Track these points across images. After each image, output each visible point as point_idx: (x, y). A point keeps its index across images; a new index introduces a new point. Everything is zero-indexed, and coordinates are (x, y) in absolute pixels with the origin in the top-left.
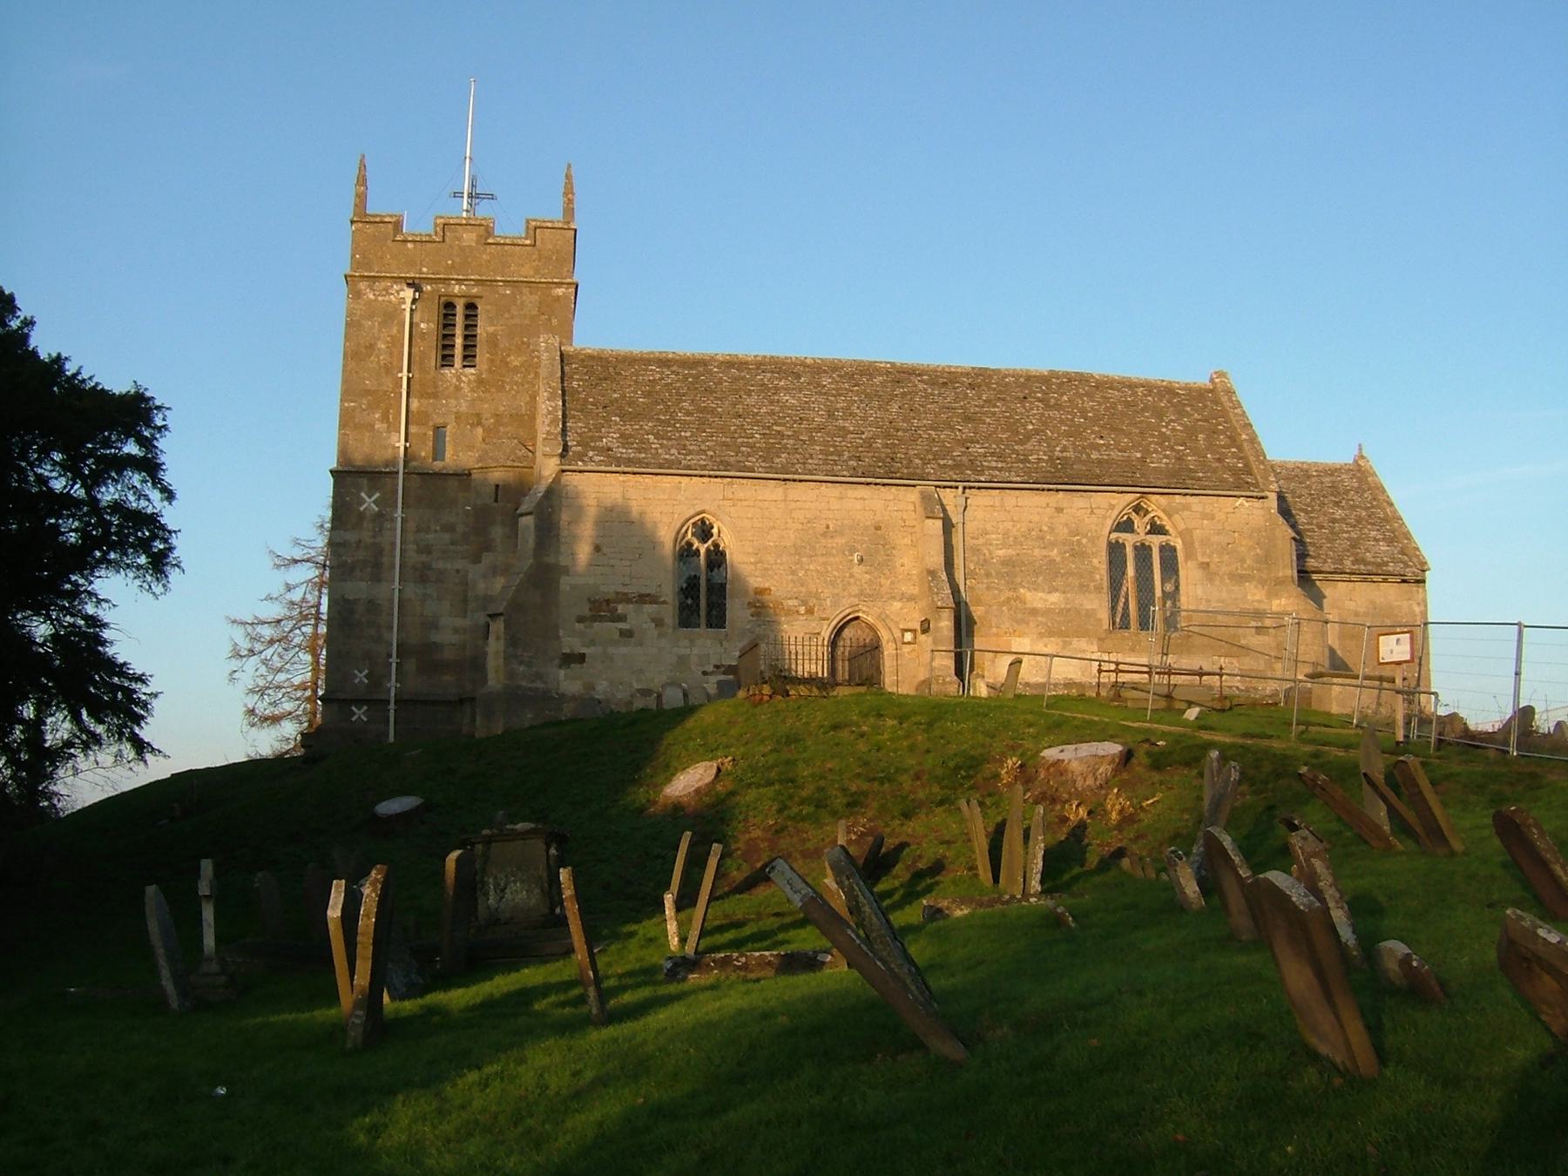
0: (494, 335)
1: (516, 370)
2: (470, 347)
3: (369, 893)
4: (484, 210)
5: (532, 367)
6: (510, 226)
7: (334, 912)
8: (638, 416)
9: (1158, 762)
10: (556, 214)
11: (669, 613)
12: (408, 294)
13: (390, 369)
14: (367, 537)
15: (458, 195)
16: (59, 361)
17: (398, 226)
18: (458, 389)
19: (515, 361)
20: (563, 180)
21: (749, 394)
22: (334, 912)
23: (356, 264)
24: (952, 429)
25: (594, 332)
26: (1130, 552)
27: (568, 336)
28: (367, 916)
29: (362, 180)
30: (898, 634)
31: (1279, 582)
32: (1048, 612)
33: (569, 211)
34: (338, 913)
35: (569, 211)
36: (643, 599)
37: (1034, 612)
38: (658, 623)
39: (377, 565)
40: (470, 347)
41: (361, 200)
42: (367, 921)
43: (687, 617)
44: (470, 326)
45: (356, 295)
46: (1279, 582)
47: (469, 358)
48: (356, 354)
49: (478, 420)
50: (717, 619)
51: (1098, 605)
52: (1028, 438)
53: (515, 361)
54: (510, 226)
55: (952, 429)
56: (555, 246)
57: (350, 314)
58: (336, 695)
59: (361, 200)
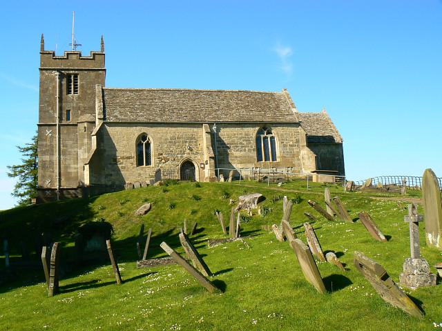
0: (83, 84)
1: (89, 94)
2: (75, 88)
3: (54, 251)
4: (78, 49)
5: (94, 93)
6: (86, 54)
7: (43, 255)
8: (124, 107)
9: (64, 114)
10: (98, 50)
11: (134, 160)
12: (58, 73)
13: (54, 95)
14: (48, 143)
15: (71, 44)
16: (16, 171)
17: (54, 54)
18: (73, 100)
19: (89, 92)
20: (40, 44)
21: (155, 99)
22: (43, 255)
23: (42, 65)
24: (212, 107)
25: (111, 83)
26: (269, 139)
27: (103, 84)
28: (53, 257)
29: (43, 41)
30: (199, 165)
31: (303, 146)
32: (240, 157)
33: (103, 49)
34: (44, 256)
35: (103, 49)
36: (129, 158)
37: (236, 157)
38: (132, 164)
39: (52, 151)
40: (75, 88)
41: (42, 47)
42: (53, 258)
43: (140, 163)
44: (76, 82)
45: (42, 74)
46: (303, 146)
47: (75, 91)
48: (43, 91)
49: (79, 109)
50: (148, 163)
51: (254, 154)
52: (233, 109)
53: (89, 92)
54: (86, 54)
55: (212, 107)
56: (98, 57)
57: (41, 79)
58: (36, 189)
59: (42, 47)
